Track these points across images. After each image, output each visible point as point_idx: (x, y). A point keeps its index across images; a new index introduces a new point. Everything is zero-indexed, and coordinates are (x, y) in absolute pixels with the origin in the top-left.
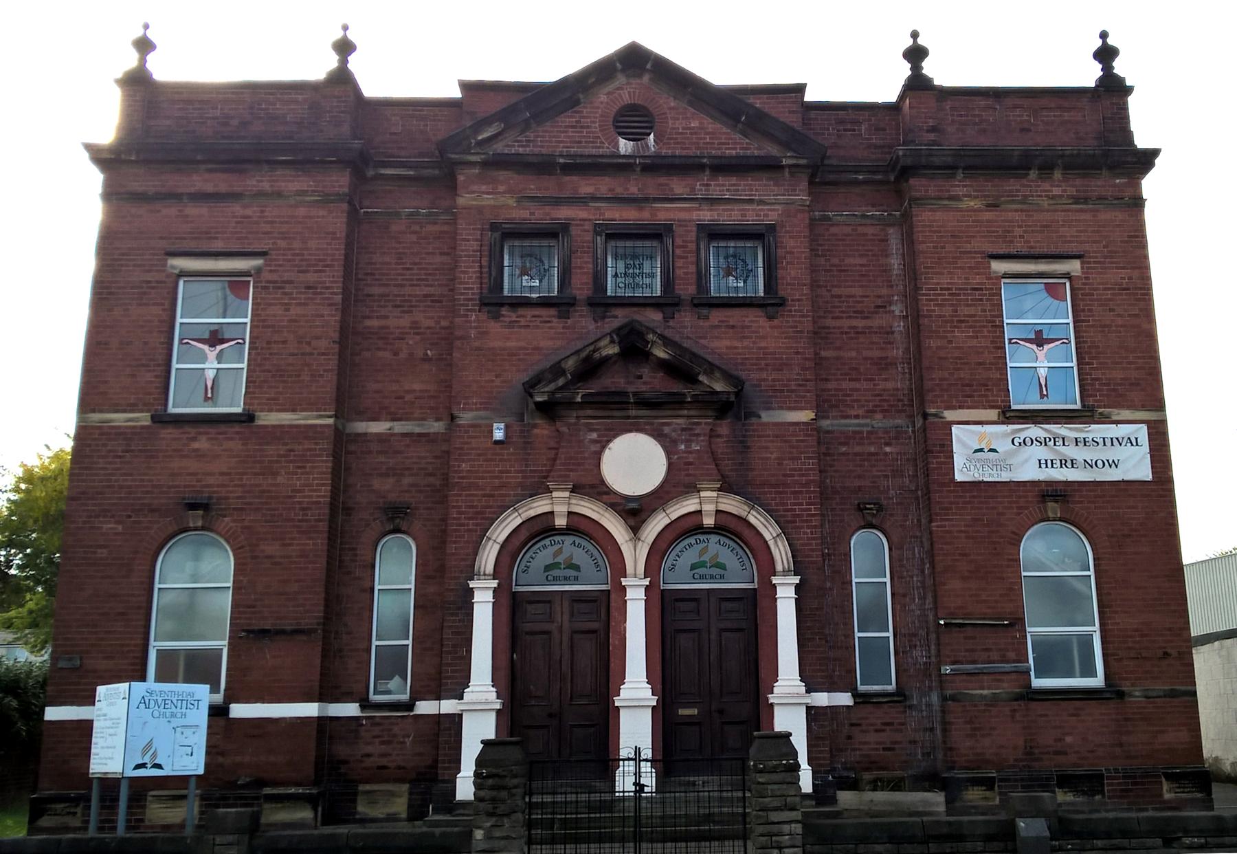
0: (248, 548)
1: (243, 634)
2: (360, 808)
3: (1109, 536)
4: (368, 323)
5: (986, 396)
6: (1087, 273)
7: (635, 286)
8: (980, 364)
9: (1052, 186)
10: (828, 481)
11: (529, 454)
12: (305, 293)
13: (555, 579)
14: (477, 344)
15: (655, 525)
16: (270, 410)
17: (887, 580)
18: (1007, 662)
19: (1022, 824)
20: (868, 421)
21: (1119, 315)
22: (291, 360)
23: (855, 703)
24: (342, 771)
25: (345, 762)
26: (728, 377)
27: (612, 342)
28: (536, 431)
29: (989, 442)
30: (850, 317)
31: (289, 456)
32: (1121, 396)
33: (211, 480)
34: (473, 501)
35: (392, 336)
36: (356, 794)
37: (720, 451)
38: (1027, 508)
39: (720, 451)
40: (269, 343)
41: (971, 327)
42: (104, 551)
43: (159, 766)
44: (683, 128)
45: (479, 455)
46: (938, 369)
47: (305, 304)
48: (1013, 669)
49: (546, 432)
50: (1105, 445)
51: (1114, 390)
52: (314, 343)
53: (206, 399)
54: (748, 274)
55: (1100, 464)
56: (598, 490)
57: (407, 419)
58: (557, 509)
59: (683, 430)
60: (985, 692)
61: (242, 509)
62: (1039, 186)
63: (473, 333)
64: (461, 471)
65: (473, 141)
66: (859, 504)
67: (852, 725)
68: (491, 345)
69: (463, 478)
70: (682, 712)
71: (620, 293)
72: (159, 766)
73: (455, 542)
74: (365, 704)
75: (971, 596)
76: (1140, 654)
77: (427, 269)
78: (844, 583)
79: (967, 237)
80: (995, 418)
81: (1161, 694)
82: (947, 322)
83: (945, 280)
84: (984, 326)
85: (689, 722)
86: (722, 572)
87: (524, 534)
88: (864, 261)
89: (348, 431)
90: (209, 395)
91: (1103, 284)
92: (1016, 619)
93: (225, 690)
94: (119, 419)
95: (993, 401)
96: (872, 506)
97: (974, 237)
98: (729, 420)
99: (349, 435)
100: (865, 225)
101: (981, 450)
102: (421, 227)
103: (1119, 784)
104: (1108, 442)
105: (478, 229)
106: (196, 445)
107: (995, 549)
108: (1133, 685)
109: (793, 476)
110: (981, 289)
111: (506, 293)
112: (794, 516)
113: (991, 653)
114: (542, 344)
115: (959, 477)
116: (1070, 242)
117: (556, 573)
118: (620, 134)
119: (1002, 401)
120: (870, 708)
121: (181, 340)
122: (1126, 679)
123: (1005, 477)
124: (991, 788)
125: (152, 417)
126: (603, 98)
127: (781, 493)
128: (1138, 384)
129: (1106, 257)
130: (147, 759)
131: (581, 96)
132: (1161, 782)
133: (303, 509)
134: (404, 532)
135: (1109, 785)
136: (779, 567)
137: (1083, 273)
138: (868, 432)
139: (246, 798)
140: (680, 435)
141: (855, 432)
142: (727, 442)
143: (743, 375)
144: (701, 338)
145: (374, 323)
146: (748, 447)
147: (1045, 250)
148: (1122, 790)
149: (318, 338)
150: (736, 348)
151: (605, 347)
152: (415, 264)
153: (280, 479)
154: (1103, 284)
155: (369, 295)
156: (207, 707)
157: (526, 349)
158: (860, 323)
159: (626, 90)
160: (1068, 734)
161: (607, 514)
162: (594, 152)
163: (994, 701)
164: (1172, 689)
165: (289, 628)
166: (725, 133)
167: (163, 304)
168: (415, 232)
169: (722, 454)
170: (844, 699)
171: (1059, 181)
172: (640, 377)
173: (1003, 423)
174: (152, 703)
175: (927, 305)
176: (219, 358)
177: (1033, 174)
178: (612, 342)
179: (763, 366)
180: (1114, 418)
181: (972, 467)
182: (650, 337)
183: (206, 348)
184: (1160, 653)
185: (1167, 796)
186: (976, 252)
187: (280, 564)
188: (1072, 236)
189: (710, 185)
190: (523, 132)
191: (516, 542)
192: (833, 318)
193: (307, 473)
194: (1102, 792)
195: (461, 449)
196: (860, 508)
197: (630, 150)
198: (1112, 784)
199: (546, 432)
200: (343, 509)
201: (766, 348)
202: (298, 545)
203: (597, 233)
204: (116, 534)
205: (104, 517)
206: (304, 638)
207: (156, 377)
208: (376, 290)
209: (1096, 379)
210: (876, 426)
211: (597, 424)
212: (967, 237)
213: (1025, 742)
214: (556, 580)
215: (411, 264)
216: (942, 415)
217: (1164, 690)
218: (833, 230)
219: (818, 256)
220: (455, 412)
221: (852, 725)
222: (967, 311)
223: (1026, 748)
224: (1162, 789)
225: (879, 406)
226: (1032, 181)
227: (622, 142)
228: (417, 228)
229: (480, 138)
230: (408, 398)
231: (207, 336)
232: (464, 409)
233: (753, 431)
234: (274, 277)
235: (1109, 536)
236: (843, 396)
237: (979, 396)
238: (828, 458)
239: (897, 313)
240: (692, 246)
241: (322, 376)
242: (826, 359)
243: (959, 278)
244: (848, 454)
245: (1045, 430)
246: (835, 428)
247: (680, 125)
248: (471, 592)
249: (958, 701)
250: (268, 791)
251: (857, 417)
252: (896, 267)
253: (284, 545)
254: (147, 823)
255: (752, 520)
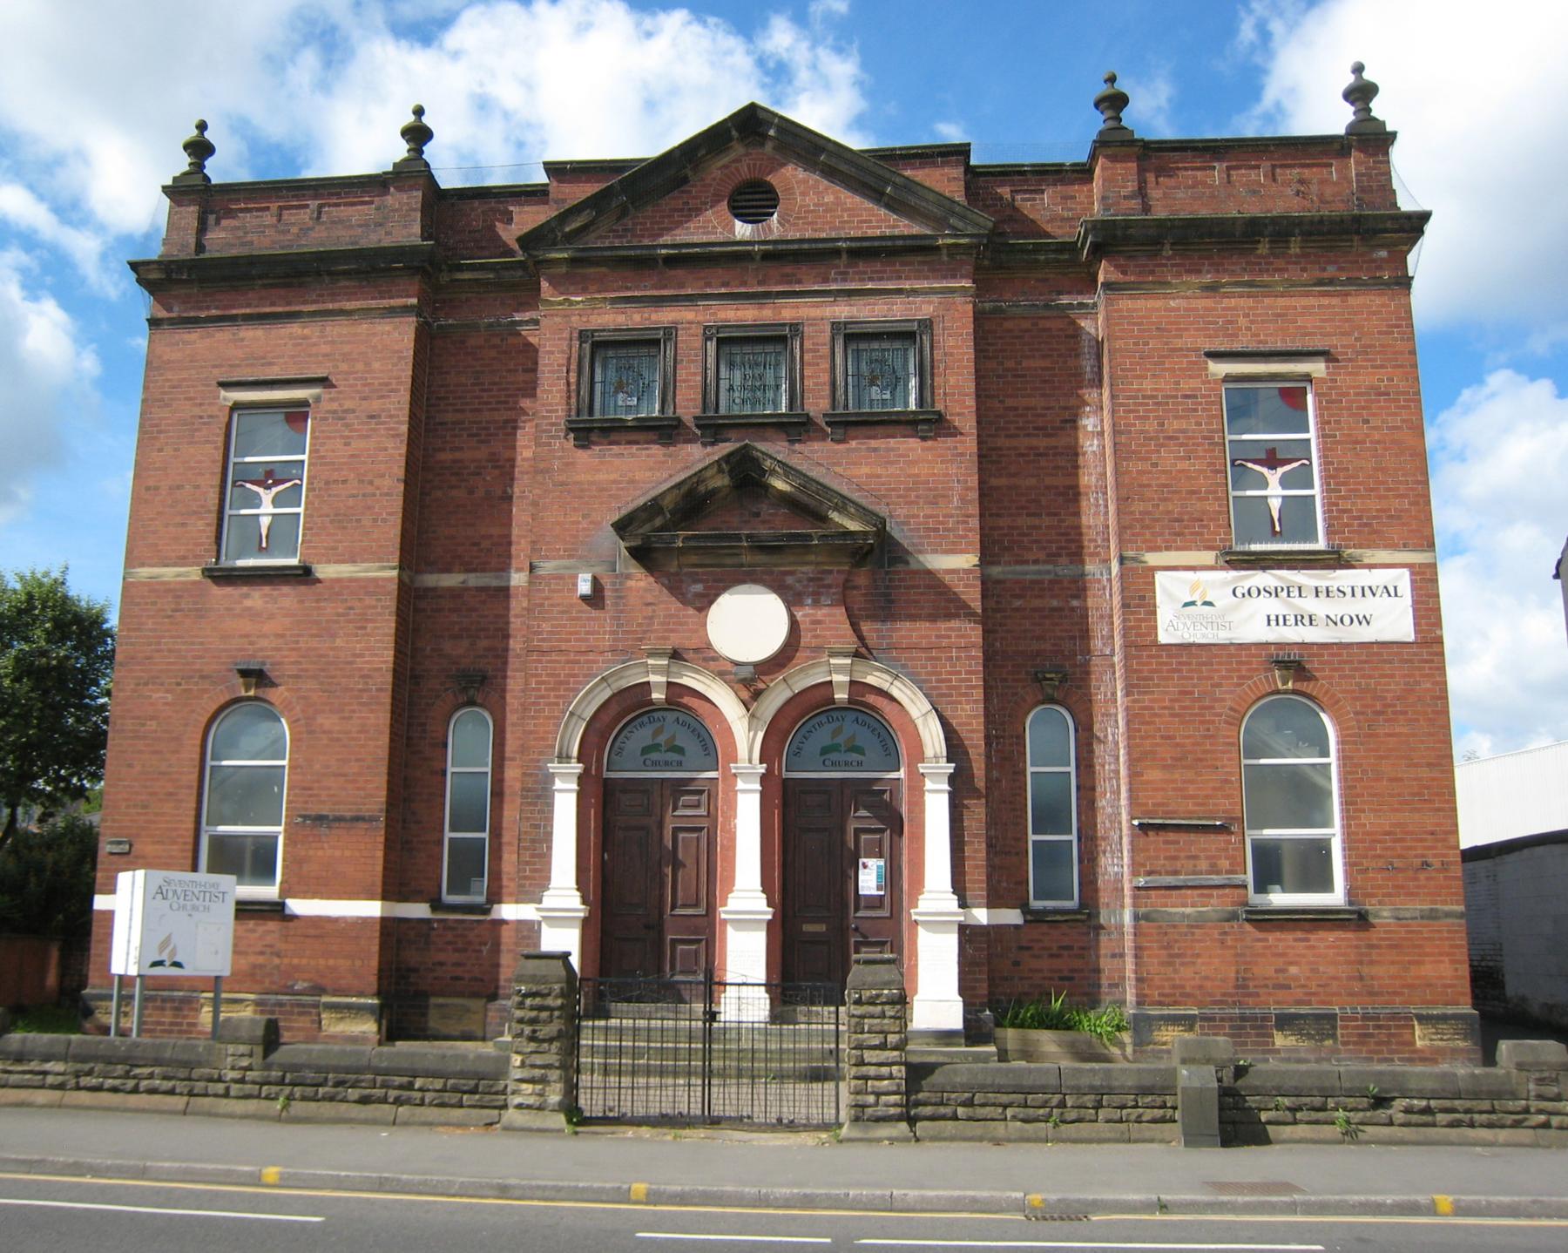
0: (303, 722)
1: (299, 820)
2: (432, 1024)
3: (1356, 713)
4: (442, 456)
5: (1202, 534)
6: (1334, 374)
7: (755, 402)
8: (1194, 492)
9: (1288, 263)
10: (998, 644)
11: (622, 612)
12: (367, 423)
13: (654, 763)
14: (563, 478)
15: (776, 697)
16: (329, 562)
17: (1072, 769)
18: (1218, 873)
19: (1185, 1072)
20: (1050, 567)
21: (1374, 428)
22: (351, 502)
23: (1025, 921)
24: (412, 980)
25: (416, 970)
26: (864, 513)
27: (720, 471)
28: (631, 583)
29: (1203, 594)
30: (1028, 435)
31: (348, 614)
32: (1376, 532)
33: (264, 643)
34: (555, 669)
35: (465, 471)
36: (427, 1007)
37: (856, 606)
38: (1251, 678)
39: (856, 606)
40: (327, 483)
41: (1182, 445)
42: (154, 723)
43: (177, 965)
44: (815, 205)
45: (562, 612)
46: (1139, 500)
47: (368, 437)
48: (1226, 882)
49: (642, 584)
50: (1353, 595)
51: (1366, 525)
52: (377, 482)
53: (261, 549)
54: (896, 383)
55: (1347, 620)
56: (705, 656)
57: (484, 570)
58: (836, 678)
59: (811, 580)
60: (1189, 910)
61: (297, 677)
62: (1272, 263)
63: (556, 464)
64: (540, 633)
65: (559, 234)
66: (1036, 674)
67: (1021, 948)
68: (577, 478)
69: (543, 640)
70: (808, 928)
71: (736, 411)
72: (177, 965)
73: (533, 718)
74: (437, 905)
75: (1174, 789)
76: (1391, 864)
77: (507, 389)
78: (1015, 773)
79: (1177, 330)
80: (1212, 562)
81: (1418, 914)
82: (1151, 439)
83: (1148, 385)
84: (1198, 445)
85: (815, 940)
86: (860, 758)
87: (614, 709)
88: (1046, 363)
89: (417, 585)
90: (264, 545)
91: (1354, 387)
92: (1232, 818)
93: (281, 883)
94: (169, 573)
95: (1208, 540)
96: (1053, 675)
97: (1186, 329)
98: (868, 568)
99: (417, 589)
100: (1048, 318)
101: (1193, 603)
102: (502, 340)
103: (1357, 1027)
104: (1358, 592)
105: (564, 339)
106: (248, 603)
107: (1208, 730)
108: (1380, 903)
109: (949, 637)
110: (1195, 397)
111: (723, 411)
112: (949, 688)
113: (1198, 862)
114: (638, 476)
115: (1163, 638)
116: (1314, 334)
117: (654, 756)
118: (737, 216)
119: (1221, 540)
120: (1044, 928)
121: (234, 482)
122: (1372, 895)
123: (1222, 637)
124: (1191, 1029)
125: (204, 571)
126: (717, 174)
127: (932, 659)
128: (1399, 517)
129: (1358, 353)
130: (164, 957)
131: (690, 173)
132: (1413, 1026)
133: (363, 677)
134: (481, 706)
135: (1343, 1027)
136: (929, 752)
137: (1328, 374)
138: (1050, 581)
139: (303, 1006)
140: (807, 586)
141: (1032, 582)
142: (865, 595)
143: (882, 510)
144: (835, 464)
145: (446, 456)
146: (892, 602)
147: (1279, 346)
148: (1360, 1035)
149: (382, 476)
150: (879, 476)
151: (712, 477)
152: (495, 384)
153: (339, 642)
154: (1354, 387)
155: (441, 424)
156: (118, 891)
157: (619, 482)
158: (1042, 443)
159: (739, 162)
160: (1291, 963)
161: (713, 685)
162: (705, 239)
163: (1199, 922)
164: (1432, 910)
165: (348, 814)
166: (865, 209)
167: (216, 442)
168: (494, 347)
169: (860, 609)
170: (1012, 917)
171: (1297, 256)
172: (758, 515)
173: (1222, 568)
174: (170, 894)
175: (1126, 418)
176: (276, 502)
177: (1263, 248)
178: (720, 471)
179: (913, 499)
180: (1366, 561)
181: (1181, 626)
182: (768, 464)
183: (1264, 470)
184: (1418, 862)
185: (1419, 1043)
186: (1188, 350)
187: (338, 740)
188: (1315, 327)
189: (847, 273)
190: (619, 219)
191: (606, 718)
192: (1007, 436)
193: (368, 635)
194: (1334, 1036)
195: (542, 605)
196: (1038, 679)
197: (748, 233)
198: (1346, 1027)
199: (642, 584)
200: (411, 677)
201: (918, 475)
202: (359, 718)
203: (708, 339)
204: (166, 704)
205: (154, 684)
206: (365, 826)
207: (208, 525)
208: (450, 417)
209: (1345, 511)
210: (1060, 573)
211: (703, 574)
212: (1177, 330)
213: (1237, 972)
214: (656, 765)
215: (490, 384)
216: (1143, 559)
217: (1421, 910)
218: (1008, 325)
219: (990, 358)
220: (536, 562)
221: (1021, 948)
222: (1176, 425)
223: (1237, 979)
224: (1414, 1034)
225: (1065, 548)
226: (1168, 258)
227: (738, 224)
228: (496, 341)
229: (567, 229)
230: (485, 544)
231: (1263, 456)
232: (547, 557)
233: (901, 580)
234: (335, 406)
235: (1356, 713)
236: (1019, 535)
237: (1192, 534)
238: (999, 615)
239: (1090, 428)
240: (826, 350)
241: (384, 520)
242: (997, 488)
243: (1166, 383)
244: (1025, 609)
245: (1280, 578)
246: (1010, 576)
247: (810, 200)
248: (550, 778)
249: (1153, 920)
250: (325, 999)
251: (1036, 562)
252: (1088, 369)
253: (344, 718)
254: (200, 1028)
255: (895, 693)
